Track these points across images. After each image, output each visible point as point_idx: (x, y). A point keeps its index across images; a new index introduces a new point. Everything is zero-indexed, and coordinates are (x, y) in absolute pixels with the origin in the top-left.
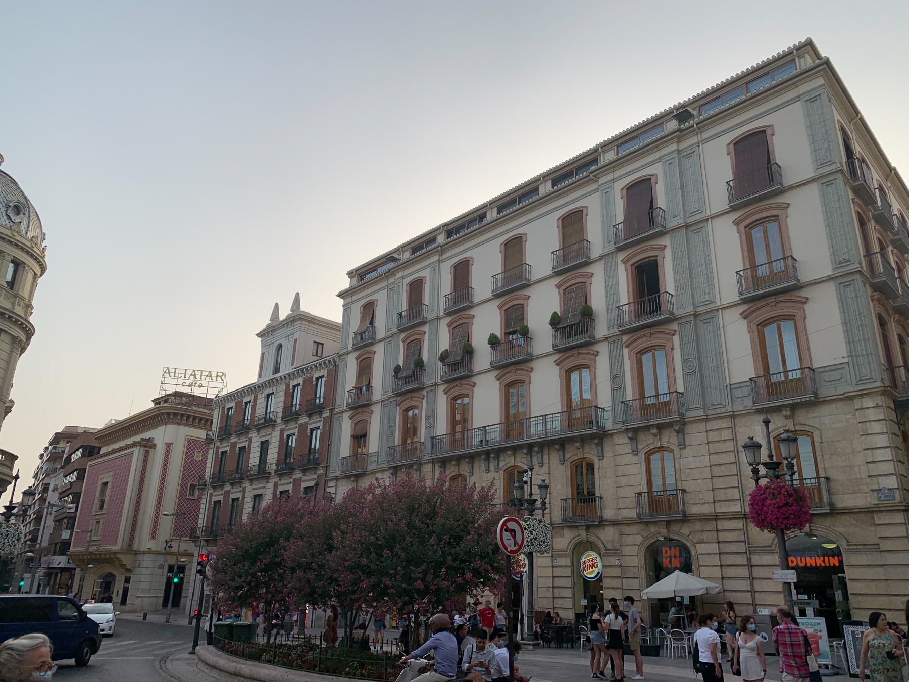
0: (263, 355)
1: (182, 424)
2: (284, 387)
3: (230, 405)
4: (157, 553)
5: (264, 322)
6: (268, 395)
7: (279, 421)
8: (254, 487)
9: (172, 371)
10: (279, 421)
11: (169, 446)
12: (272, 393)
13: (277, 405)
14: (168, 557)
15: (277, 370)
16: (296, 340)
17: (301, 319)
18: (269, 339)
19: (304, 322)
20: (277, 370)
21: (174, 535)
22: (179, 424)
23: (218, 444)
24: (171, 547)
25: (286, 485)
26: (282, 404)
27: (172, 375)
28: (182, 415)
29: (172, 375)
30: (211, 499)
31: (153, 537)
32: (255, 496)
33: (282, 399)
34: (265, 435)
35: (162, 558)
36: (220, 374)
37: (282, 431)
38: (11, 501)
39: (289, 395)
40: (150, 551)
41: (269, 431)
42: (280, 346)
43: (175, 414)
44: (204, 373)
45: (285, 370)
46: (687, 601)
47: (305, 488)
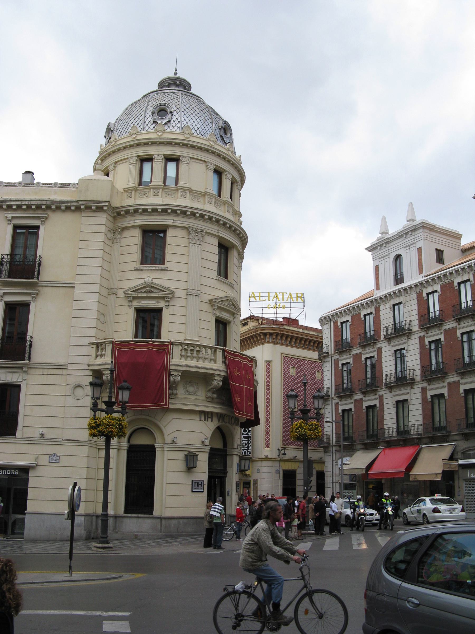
0: (377, 268)
1: (277, 343)
2: (414, 296)
3: (344, 319)
4: (273, 460)
5: (374, 237)
6: (394, 306)
7: (416, 328)
8: (393, 393)
9: (257, 294)
10: (416, 328)
11: (268, 363)
12: (401, 303)
13: (409, 313)
14: (282, 463)
15: (399, 280)
16: (420, 249)
17: (424, 227)
18: (384, 251)
19: (425, 230)
20: (399, 280)
21: (284, 444)
22: (263, 344)
23: (337, 357)
24: (285, 454)
25: (348, 404)
26: (416, 312)
27: (257, 298)
28: (277, 335)
29: (257, 298)
30: (337, 409)
31: (267, 446)
32: (397, 402)
33: (415, 307)
34: (398, 344)
35: (277, 464)
36: (300, 295)
37: (422, 339)
38: (305, 406)
39: (423, 304)
40: (267, 459)
41: (404, 339)
42: (398, 257)
43: (271, 334)
44: (285, 295)
45: (412, 278)
46: (327, 529)
47: (465, 391)
